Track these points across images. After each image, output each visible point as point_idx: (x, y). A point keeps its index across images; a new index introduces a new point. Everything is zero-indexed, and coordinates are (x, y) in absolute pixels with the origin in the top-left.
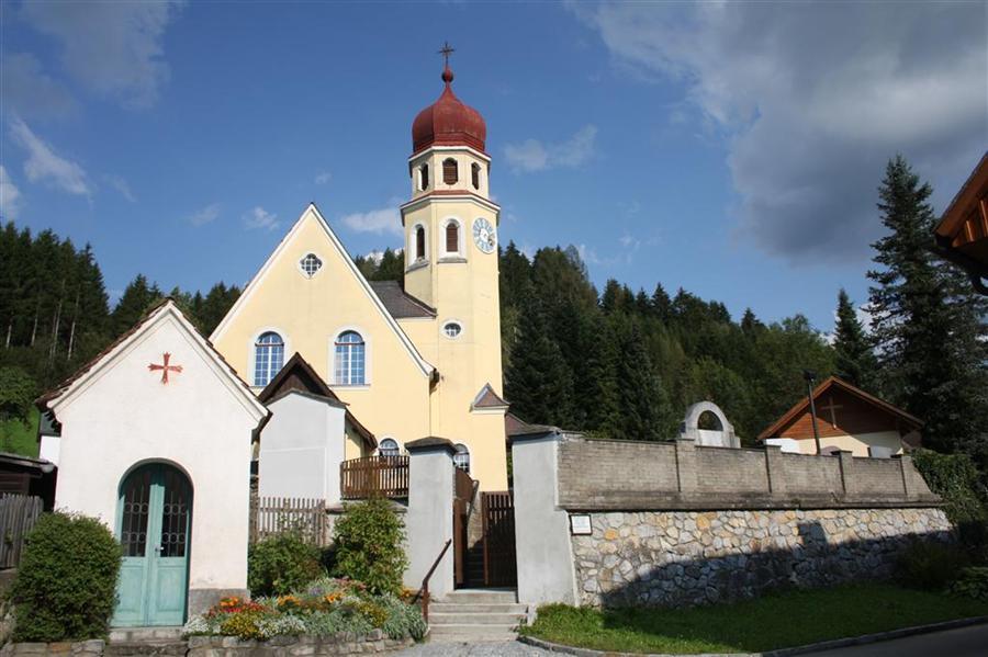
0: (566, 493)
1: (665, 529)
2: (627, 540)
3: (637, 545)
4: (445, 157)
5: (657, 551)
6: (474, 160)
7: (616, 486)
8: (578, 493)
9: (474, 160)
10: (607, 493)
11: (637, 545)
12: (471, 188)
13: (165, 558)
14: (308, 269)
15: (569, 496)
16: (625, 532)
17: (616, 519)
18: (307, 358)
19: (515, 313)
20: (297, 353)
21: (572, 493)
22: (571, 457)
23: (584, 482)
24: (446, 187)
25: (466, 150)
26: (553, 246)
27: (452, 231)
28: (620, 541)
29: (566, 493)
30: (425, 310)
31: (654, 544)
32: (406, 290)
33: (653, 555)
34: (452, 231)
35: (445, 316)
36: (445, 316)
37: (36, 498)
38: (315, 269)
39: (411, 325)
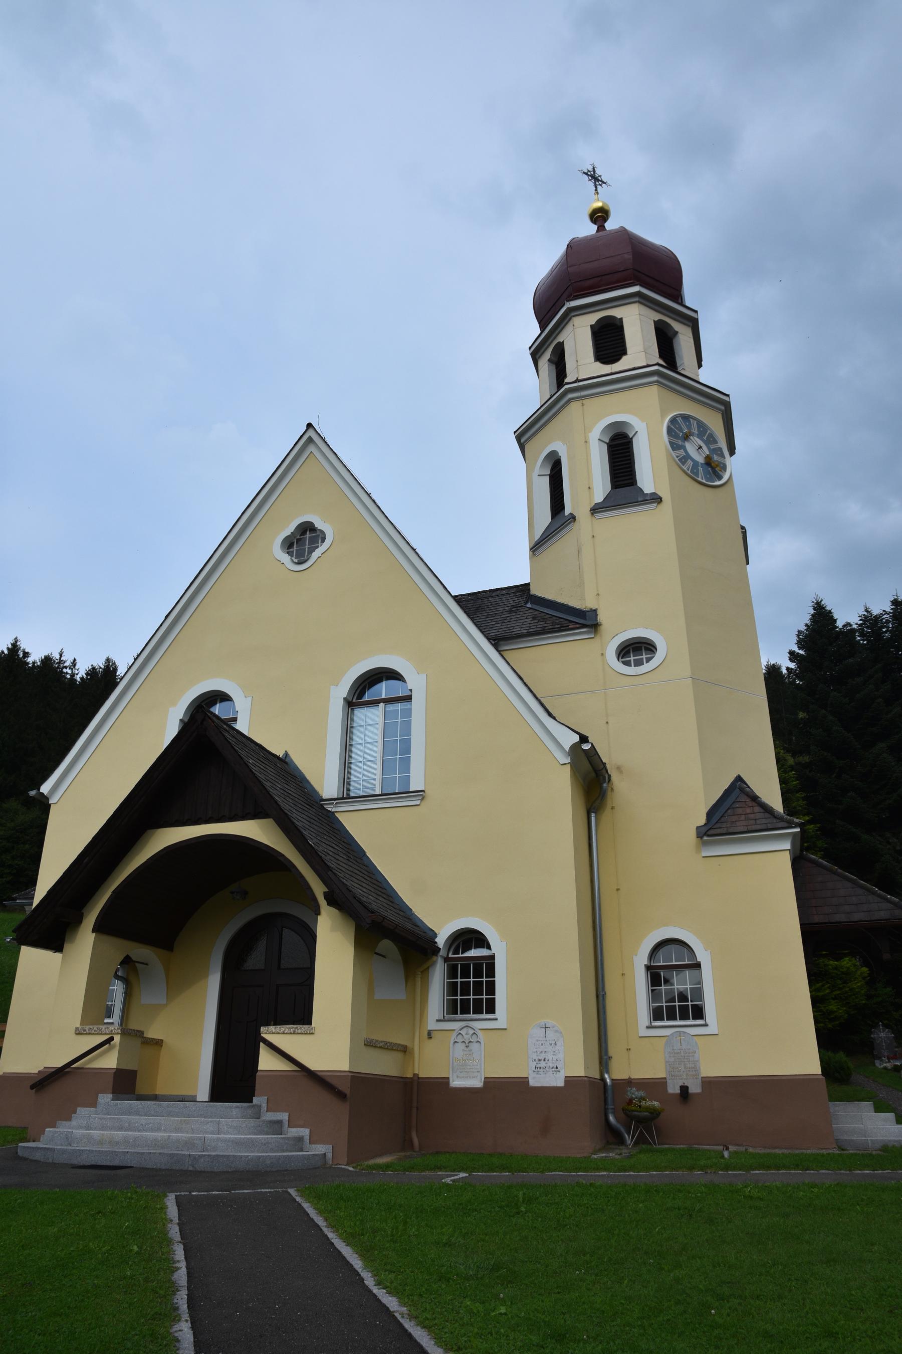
4: (593, 318)
6: (658, 317)
9: (658, 317)
20: (739, 779)
27: (620, 449)
34: (620, 449)
35: (617, 630)
36: (617, 630)
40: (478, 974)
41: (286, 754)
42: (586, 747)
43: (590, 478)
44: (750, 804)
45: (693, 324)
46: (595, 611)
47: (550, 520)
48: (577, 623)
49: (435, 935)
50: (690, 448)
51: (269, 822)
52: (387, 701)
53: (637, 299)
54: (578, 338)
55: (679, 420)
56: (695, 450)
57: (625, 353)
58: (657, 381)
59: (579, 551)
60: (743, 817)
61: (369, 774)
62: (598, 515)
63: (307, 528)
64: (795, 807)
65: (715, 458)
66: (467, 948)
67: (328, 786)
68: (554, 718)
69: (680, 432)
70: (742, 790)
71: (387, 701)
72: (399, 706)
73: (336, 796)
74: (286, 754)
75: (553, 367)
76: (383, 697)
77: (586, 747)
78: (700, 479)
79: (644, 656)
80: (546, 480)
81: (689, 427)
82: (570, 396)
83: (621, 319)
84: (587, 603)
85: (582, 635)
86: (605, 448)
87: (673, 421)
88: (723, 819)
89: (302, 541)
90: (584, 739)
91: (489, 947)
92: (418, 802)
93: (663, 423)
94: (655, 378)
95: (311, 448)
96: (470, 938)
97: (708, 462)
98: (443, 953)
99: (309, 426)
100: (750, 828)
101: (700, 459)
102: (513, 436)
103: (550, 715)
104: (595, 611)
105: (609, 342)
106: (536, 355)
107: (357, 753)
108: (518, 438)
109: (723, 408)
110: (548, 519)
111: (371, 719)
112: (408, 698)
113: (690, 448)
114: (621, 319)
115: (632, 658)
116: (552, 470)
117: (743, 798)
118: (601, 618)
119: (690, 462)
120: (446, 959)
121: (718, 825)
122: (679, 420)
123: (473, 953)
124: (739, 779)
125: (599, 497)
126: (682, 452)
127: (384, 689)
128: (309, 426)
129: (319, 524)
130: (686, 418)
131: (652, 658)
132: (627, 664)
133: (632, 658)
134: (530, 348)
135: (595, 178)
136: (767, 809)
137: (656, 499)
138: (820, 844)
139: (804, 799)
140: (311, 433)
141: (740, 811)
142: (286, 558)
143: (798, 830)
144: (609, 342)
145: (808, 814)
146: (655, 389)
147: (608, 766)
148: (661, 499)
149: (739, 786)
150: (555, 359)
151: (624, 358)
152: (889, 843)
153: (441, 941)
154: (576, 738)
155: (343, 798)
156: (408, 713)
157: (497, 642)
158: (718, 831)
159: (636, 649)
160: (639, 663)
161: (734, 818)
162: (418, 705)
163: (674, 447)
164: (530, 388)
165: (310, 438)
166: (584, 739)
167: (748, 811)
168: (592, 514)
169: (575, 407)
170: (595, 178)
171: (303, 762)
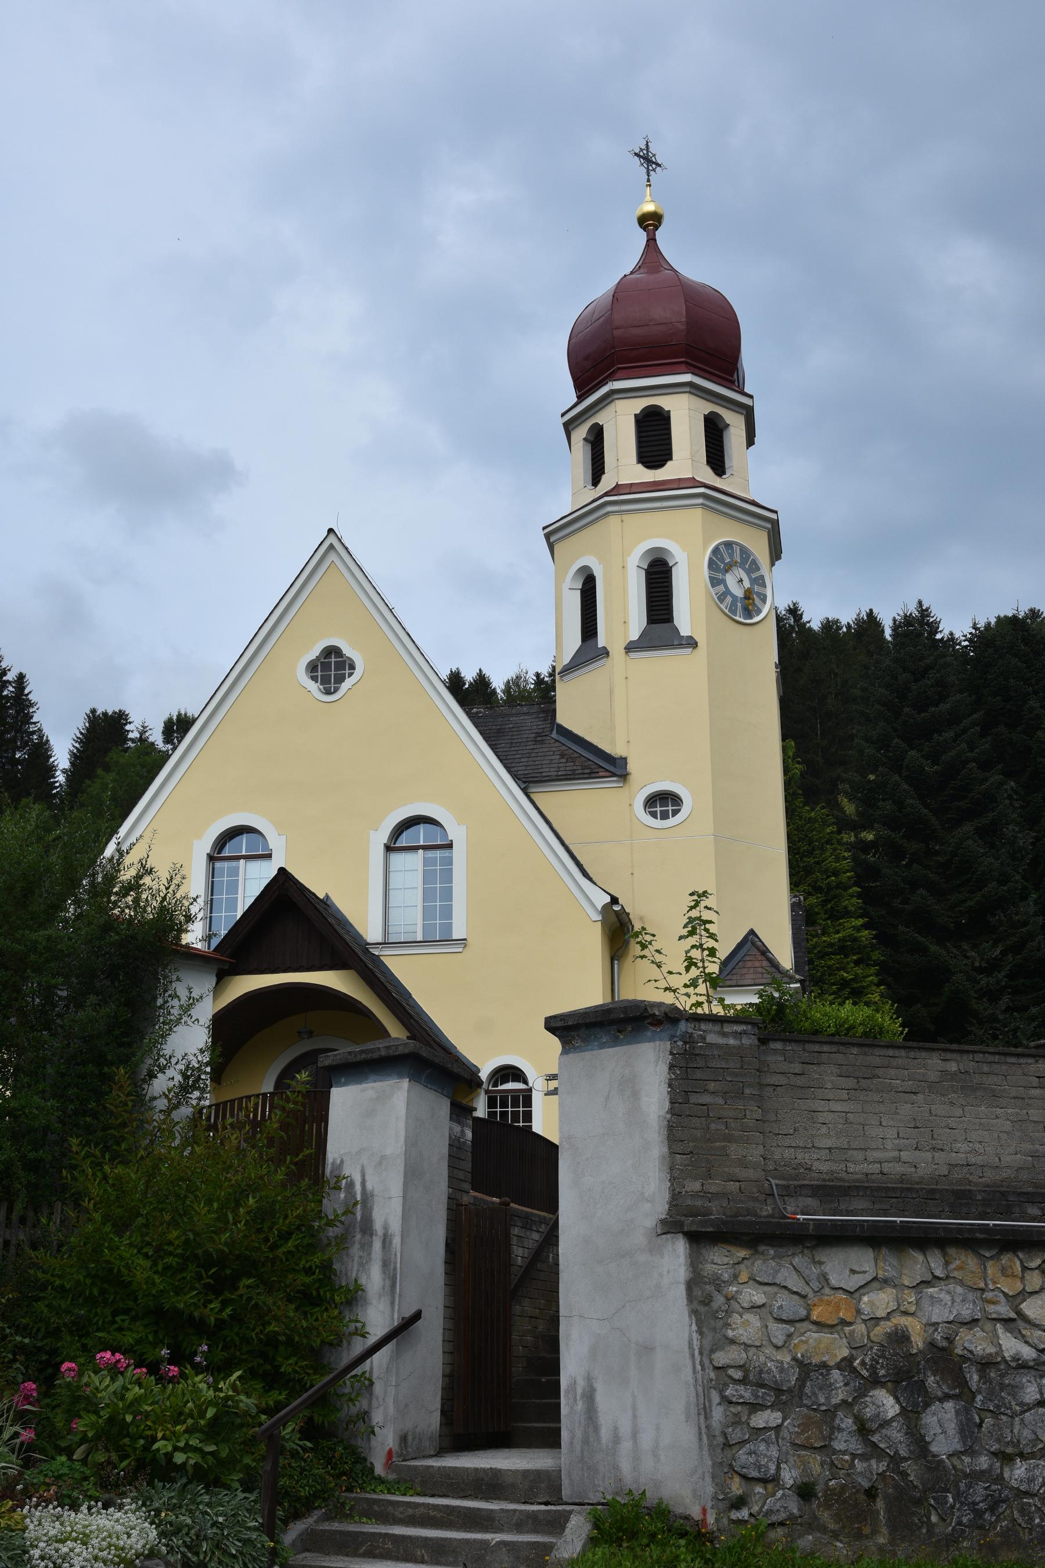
0: (696, 1186)
1: (1015, 1300)
2: (886, 1327)
3: (918, 1342)
4: (638, 405)
5: (985, 1365)
6: (708, 408)
7: (858, 1168)
8: (733, 1186)
9: (708, 408)
10: (831, 1192)
11: (918, 1342)
12: (706, 475)
13: (565, 1435)
14: (325, 680)
15: (703, 1194)
16: (879, 1301)
17: (845, 1267)
18: (316, 882)
19: (798, 769)
20: (752, 932)
21: (715, 1186)
22: (712, 1086)
23: (755, 1153)
24: (649, 475)
25: (690, 384)
26: (1037, 608)
27: (658, 576)
28: (860, 1328)
29: (696, 1186)
30: (606, 766)
31: (975, 1342)
32: (562, 719)
33: (974, 1378)
34: (658, 576)
35: (646, 780)
36: (646, 780)
37: (517, 1309)
38: (340, 679)
39: (577, 804)
40: (515, 1104)
41: (327, 896)
42: (616, 908)
43: (624, 611)
44: (760, 957)
45: (749, 414)
46: (625, 759)
47: (580, 643)
48: (607, 770)
49: (479, 1071)
50: (731, 580)
51: (352, 971)
52: (425, 848)
53: (688, 389)
54: (620, 424)
55: (722, 548)
56: (736, 583)
57: (671, 459)
58: (702, 504)
59: (611, 692)
60: (752, 970)
61: (410, 919)
62: (632, 655)
63: (331, 651)
64: (846, 907)
65: (756, 588)
66: (505, 1081)
67: (371, 931)
68: (590, 879)
69: (722, 561)
70: (753, 943)
71: (425, 848)
72: (438, 854)
73: (380, 940)
74: (327, 896)
75: (589, 447)
76: (422, 843)
77: (616, 908)
78: (737, 618)
79: (670, 808)
80: (577, 595)
81: (731, 555)
82: (609, 509)
83: (669, 411)
84: (617, 750)
85: (612, 783)
86: (643, 574)
87: (716, 551)
88: (734, 971)
89: (330, 668)
90: (614, 900)
91: (526, 1082)
92: (460, 950)
93: (705, 548)
94: (700, 501)
95: (332, 557)
96: (509, 1073)
97: (748, 595)
98: (485, 1086)
99: (331, 531)
100: (757, 981)
101: (739, 593)
102: (542, 533)
103: (586, 874)
104: (625, 759)
105: (654, 438)
106: (569, 427)
107: (394, 899)
108: (547, 536)
109: (769, 526)
110: (578, 642)
111: (410, 866)
112: (450, 846)
113: (731, 580)
114: (669, 411)
115: (658, 809)
116: (584, 584)
117: (754, 951)
118: (631, 767)
119: (729, 599)
120: (487, 1092)
121: (729, 977)
122: (722, 548)
123: (511, 1086)
124: (752, 932)
125: (634, 635)
126: (721, 588)
127: (420, 834)
128: (331, 531)
129: (348, 651)
130: (728, 545)
131: (679, 810)
132: (654, 815)
133: (658, 809)
134: (563, 415)
135: (648, 160)
136: (774, 964)
137: (691, 643)
138: (876, 955)
139: (859, 896)
140: (332, 539)
141: (749, 964)
142: (313, 687)
143: (798, 985)
144: (654, 438)
145: (861, 916)
146: (699, 511)
147: (631, 917)
148: (696, 643)
149: (751, 939)
150: (591, 438)
151: (669, 463)
152: (967, 958)
153: (484, 1075)
154: (608, 899)
155: (385, 943)
156: (449, 861)
157: (528, 780)
158: (728, 983)
159: (663, 803)
160: (665, 816)
161: (745, 971)
162: (458, 853)
163: (714, 582)
164: (566, 492)
165: (332, 544)
166: (614, 900)
167: (757, 964)
168: (626, 653)
169: (613, 521)
170: (648, 160)
171: (345, 905)
